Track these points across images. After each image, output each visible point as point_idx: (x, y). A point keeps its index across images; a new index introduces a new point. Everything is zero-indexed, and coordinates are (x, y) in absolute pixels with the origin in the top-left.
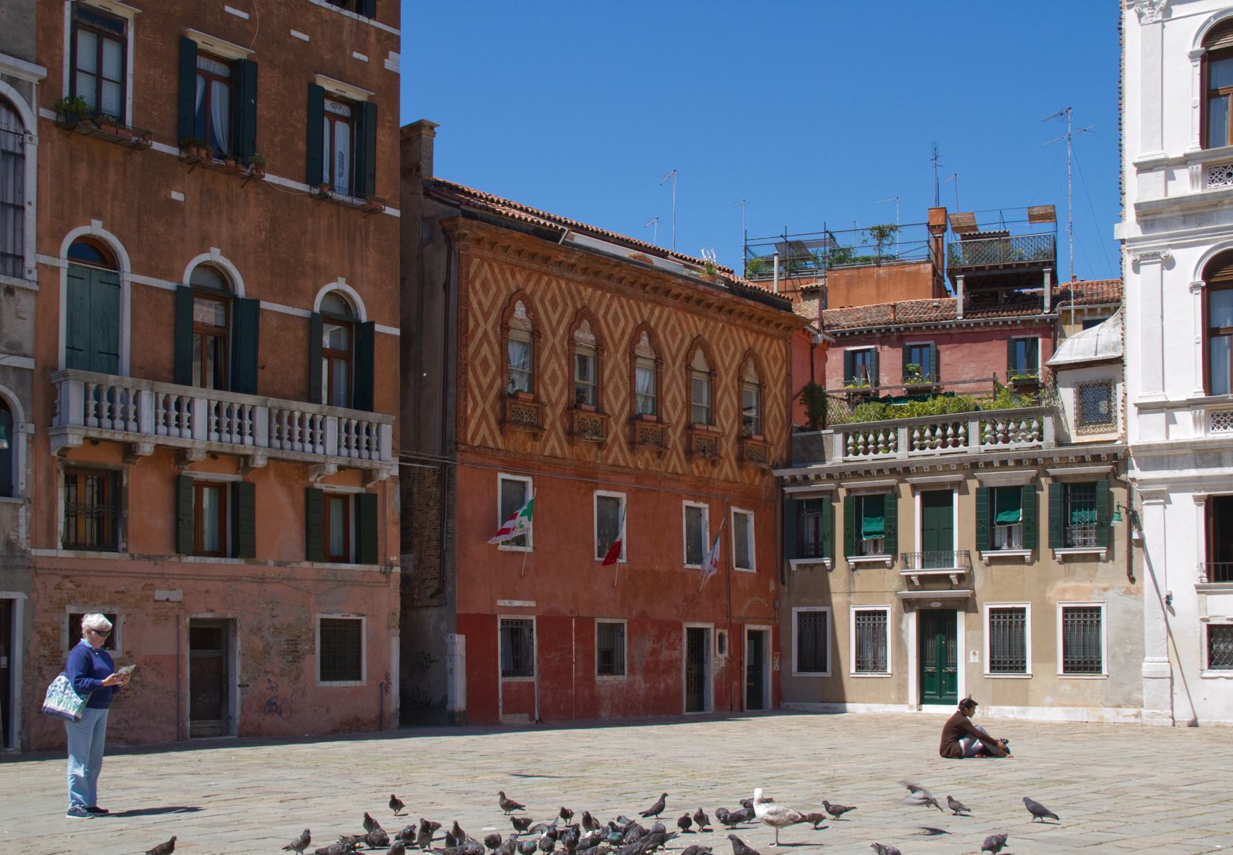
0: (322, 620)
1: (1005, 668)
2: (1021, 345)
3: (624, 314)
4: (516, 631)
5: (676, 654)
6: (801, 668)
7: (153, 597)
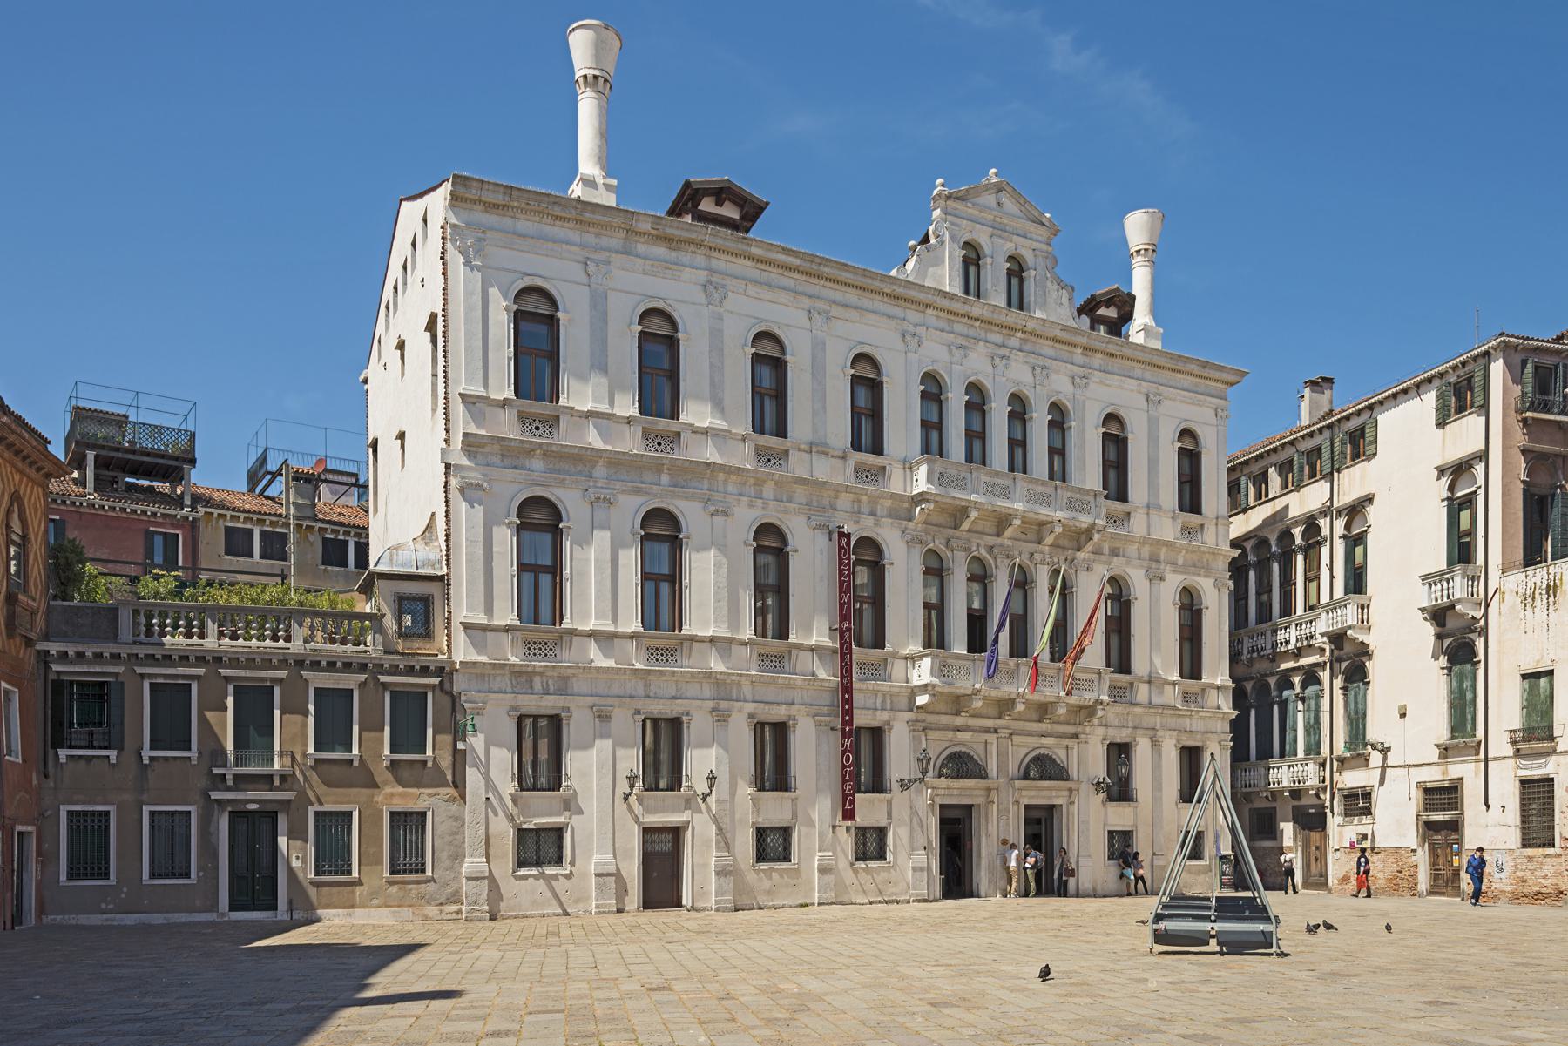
2: (158, 541)
6: (70, 876)
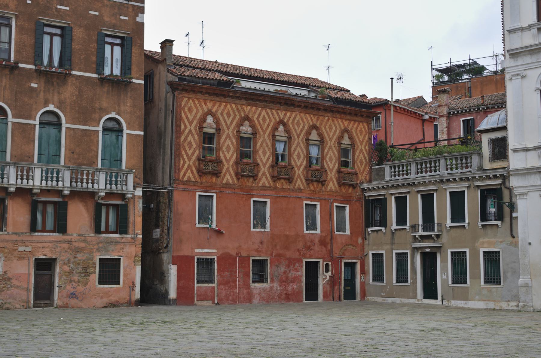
0: (100, 259)
1: (404, 281)
3: (269, 117)
5: (299, 273)
7: (17, 249)
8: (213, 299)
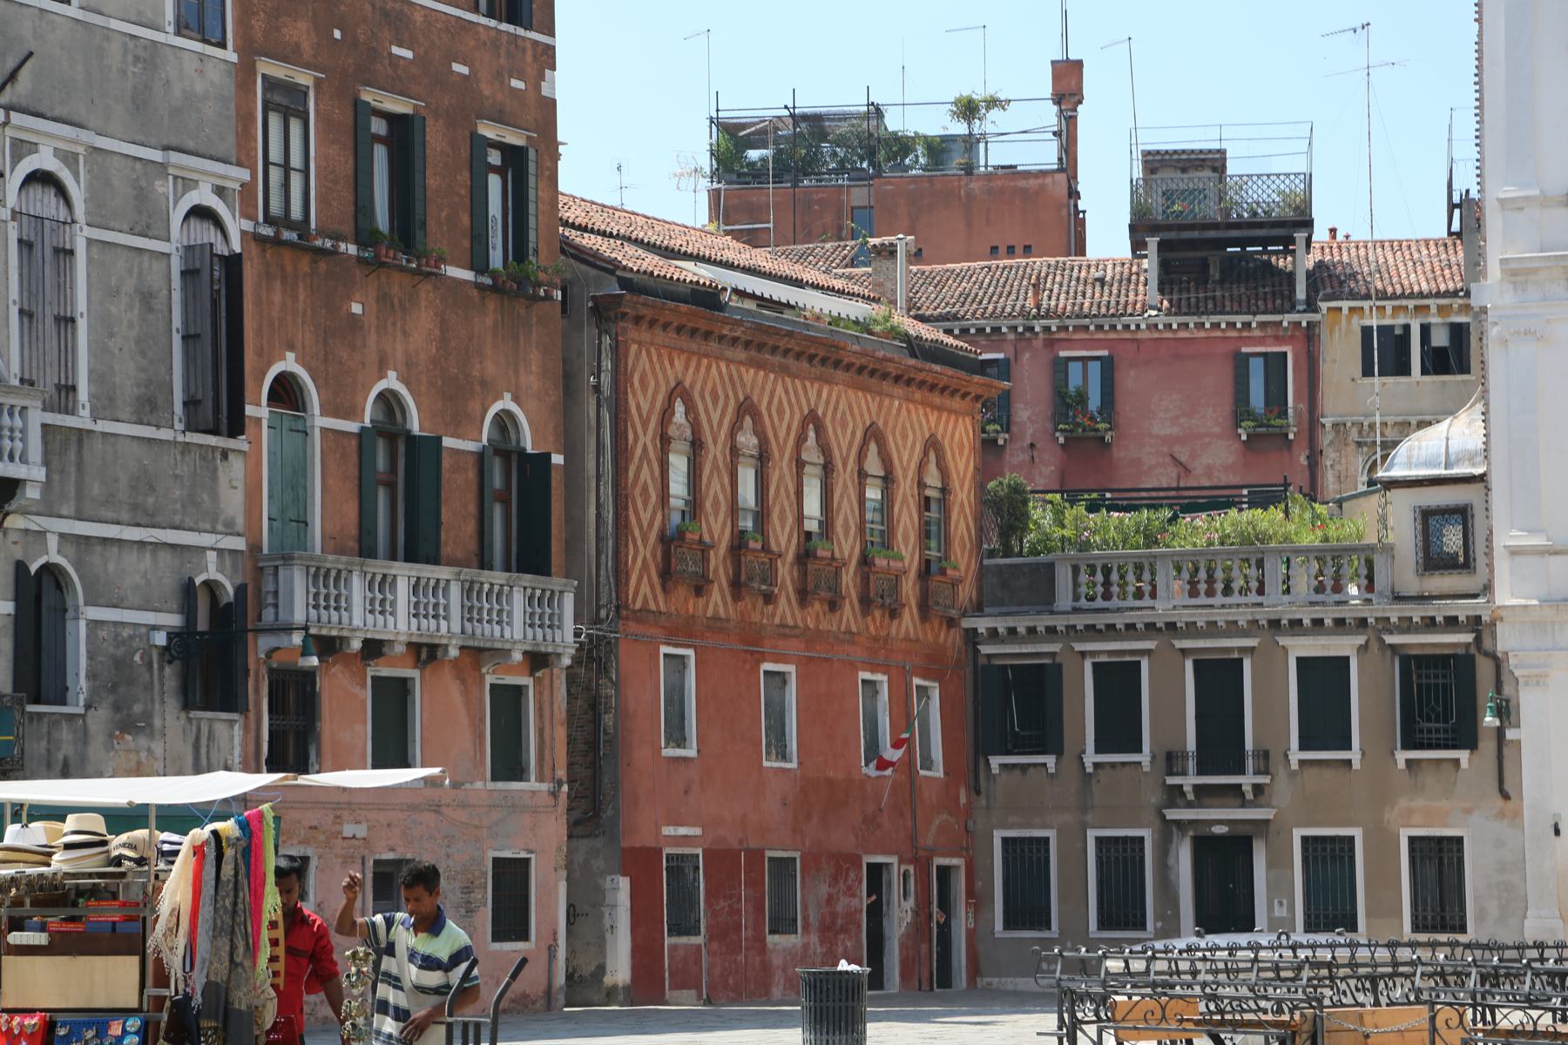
2: (1257, 369)
4: (679, 866)
6: (1008, 925)
7: (340, 832)
8: (698, 988)
